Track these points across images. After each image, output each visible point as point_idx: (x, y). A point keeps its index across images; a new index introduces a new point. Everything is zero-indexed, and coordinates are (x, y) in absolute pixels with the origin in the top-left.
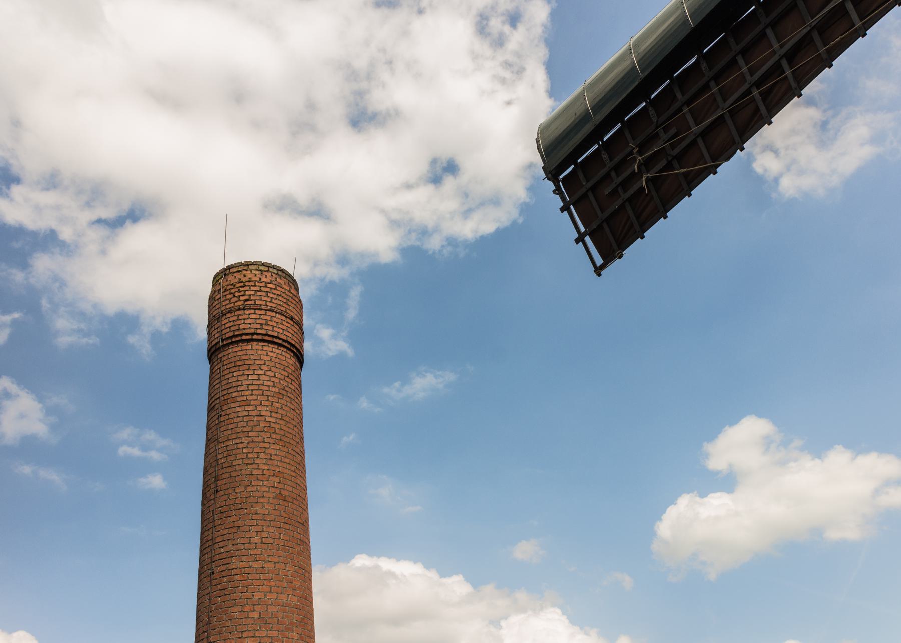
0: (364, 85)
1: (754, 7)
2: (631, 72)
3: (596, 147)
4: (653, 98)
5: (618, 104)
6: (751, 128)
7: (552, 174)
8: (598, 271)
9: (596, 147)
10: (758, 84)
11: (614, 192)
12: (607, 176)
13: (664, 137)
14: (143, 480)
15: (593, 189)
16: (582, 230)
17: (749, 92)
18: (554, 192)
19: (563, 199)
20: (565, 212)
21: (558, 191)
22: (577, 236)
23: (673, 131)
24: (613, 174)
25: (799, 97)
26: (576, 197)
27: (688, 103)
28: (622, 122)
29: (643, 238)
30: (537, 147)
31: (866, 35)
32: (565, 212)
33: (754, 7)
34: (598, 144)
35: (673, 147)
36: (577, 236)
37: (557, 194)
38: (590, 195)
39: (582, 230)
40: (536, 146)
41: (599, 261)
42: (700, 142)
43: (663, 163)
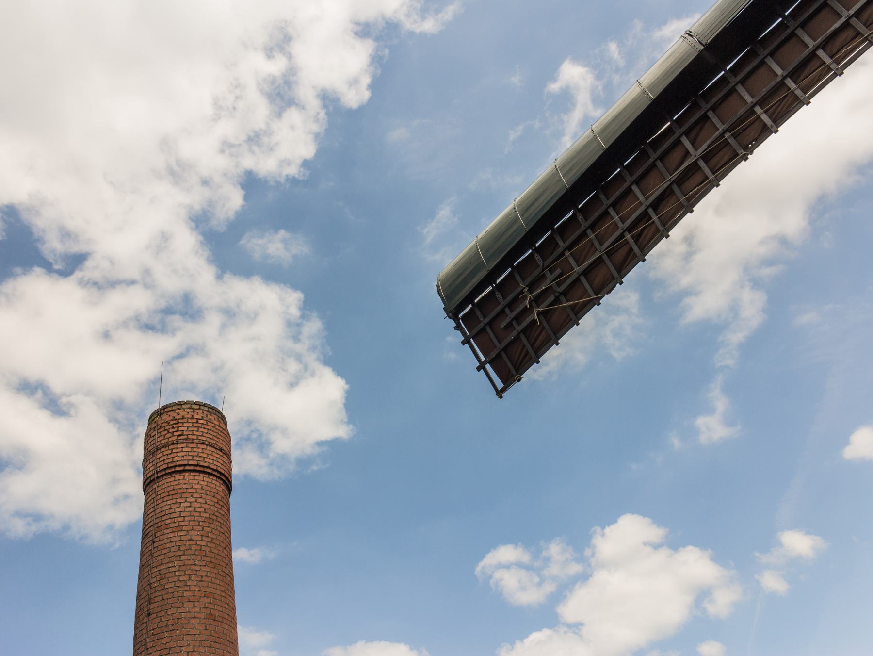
1: (619, 169)
3: (490, 288)
7: (453, 313)
8: (500, 393)
9: (490, 288)
10: (630, 229)
11: (509, 326)
12: (502, 312)
13: (550, 277)
18: (455, 328)
19: (464, 334)
20: (467, 345)
23: (558, 271)
24: (507, 310)
27: (592, 227)
30: (438, 291)
31: (810, 103)
32: (467, 345)
34: (492, 286)
35: (559, 284)
37: (458, 330)
39: (483, 358)
41: (500, 385)
43: (551, 298)
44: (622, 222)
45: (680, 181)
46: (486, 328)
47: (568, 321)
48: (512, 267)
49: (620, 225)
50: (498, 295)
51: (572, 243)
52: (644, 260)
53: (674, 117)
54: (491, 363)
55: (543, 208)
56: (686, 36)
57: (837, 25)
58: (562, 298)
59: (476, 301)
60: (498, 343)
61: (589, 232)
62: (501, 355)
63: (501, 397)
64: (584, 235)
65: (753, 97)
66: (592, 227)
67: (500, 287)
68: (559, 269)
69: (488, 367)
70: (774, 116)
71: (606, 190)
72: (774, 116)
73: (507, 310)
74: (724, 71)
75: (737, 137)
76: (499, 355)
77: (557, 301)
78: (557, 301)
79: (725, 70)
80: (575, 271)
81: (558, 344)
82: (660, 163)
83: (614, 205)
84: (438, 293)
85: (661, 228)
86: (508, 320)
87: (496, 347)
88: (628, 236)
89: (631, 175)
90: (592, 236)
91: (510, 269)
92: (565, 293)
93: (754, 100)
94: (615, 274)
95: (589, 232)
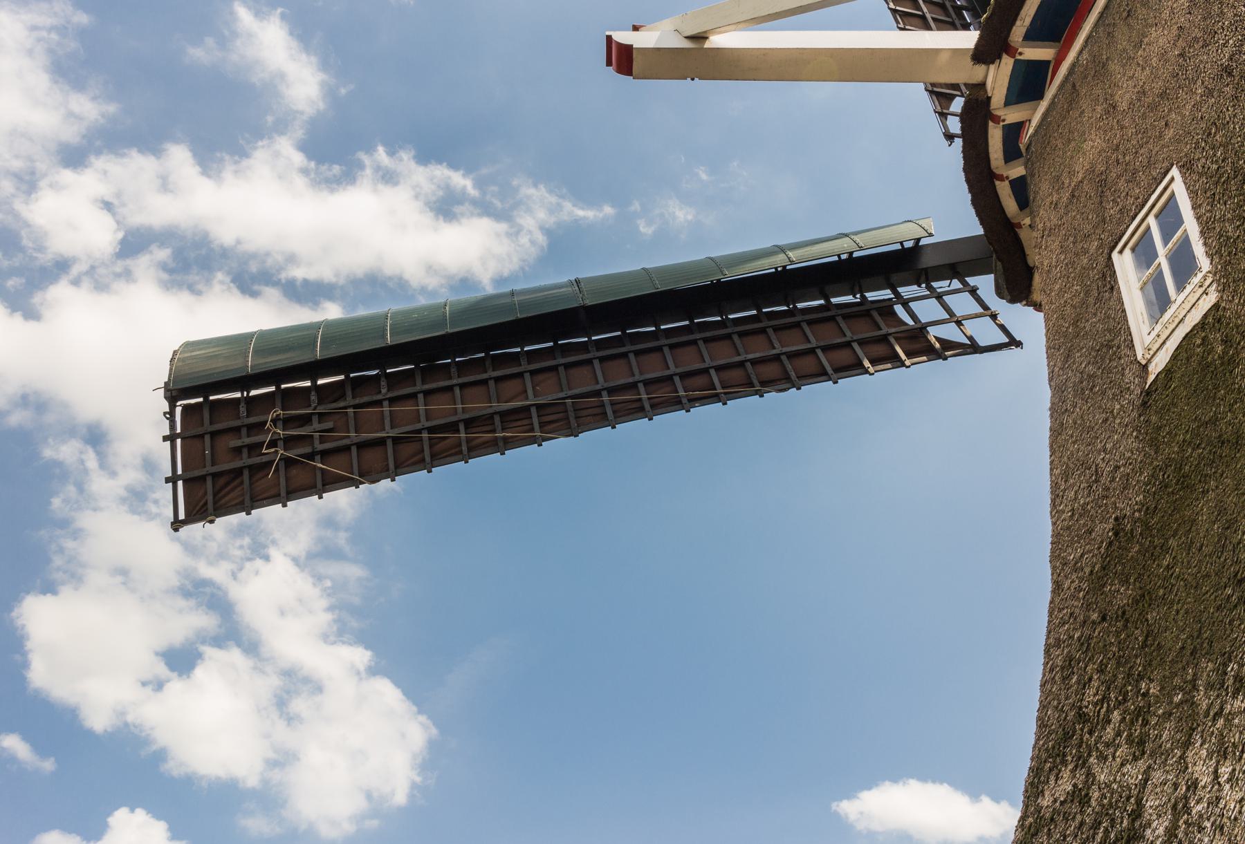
0: (1111, 29)
1: (450, 361)
2: (442, 322)
3: (238, 395)
4: (374, 369)
5: (431, 337)
6: (443, 458)
7: (174, 393)
8: (177, 525)
9: (238, 395)
10: (431, 430)
11: (238, 451)
12: (236, 430)
13: (316, 425)
14: (690, 217)
15: (214, 435)
16: (180, 472)
17: (419, 431)
18: (165, 414)
19: (172, 426)
20: (168, 443)
21: (170, 415)
22: (170, 474)
23: (329, 425)
24: (244, 431)
25: (501, 454)
26: (188, 434)
27: (392, 401)
28: (278, 387)
29: (503, 454)
30: (172, 359)
31: (578, 436)
32: (168, 443)
33: (450, 361)
34: (242, 394)
35: (322, 440)
36: (170, 474)
37: (167, 418)
38: (207, 438)
39: (180, 472)
40: (171, 357)
41: (182, 516)
42: (246, 473)
43: (308, 450)
44: (391, 426)
45: (506, 416)
46: (242, 430)
47: (453, 451)
48: (487, 354)
49: (423, 418)
50: (243, 409)
51: (545, 368)
52: (614, 427)
53: (663, 325)
54: (185, 482)
55: (207, 370)
56: (575, 284)
57: (839, 341)
58: (318, 457)
59: (283, 386)
60: (673, 366)
61: (386, 403)
62: (205, 480)
63: (176, 530)
64: (379, 403)
65: (676, 367)
66: (392, 401)
67: (250, 401)
68: (332, 423)
69: (180, 483)
70: (457, 450)
71: (429, 372)
72: (457, 450)
73: (244, 431)
74: (312, 383)
75: (541, 416)
76: (202, 479)
77: (311, 456)
78: (311, 456)
79: (658, 329)
80: (491, 406)
81: (285, 505)
82: (529, 377)
83: (427, 393)
84: (171, 361)
85: (428, 459)
86: (238, 443)
87: (419, 422)
88: (425, 435)
89: (424, 382)
90: (386, 409)
91: (201, 400)
92: (325, 454)
93: (606, 385)
94: (283, 493)
95: (386, 403)
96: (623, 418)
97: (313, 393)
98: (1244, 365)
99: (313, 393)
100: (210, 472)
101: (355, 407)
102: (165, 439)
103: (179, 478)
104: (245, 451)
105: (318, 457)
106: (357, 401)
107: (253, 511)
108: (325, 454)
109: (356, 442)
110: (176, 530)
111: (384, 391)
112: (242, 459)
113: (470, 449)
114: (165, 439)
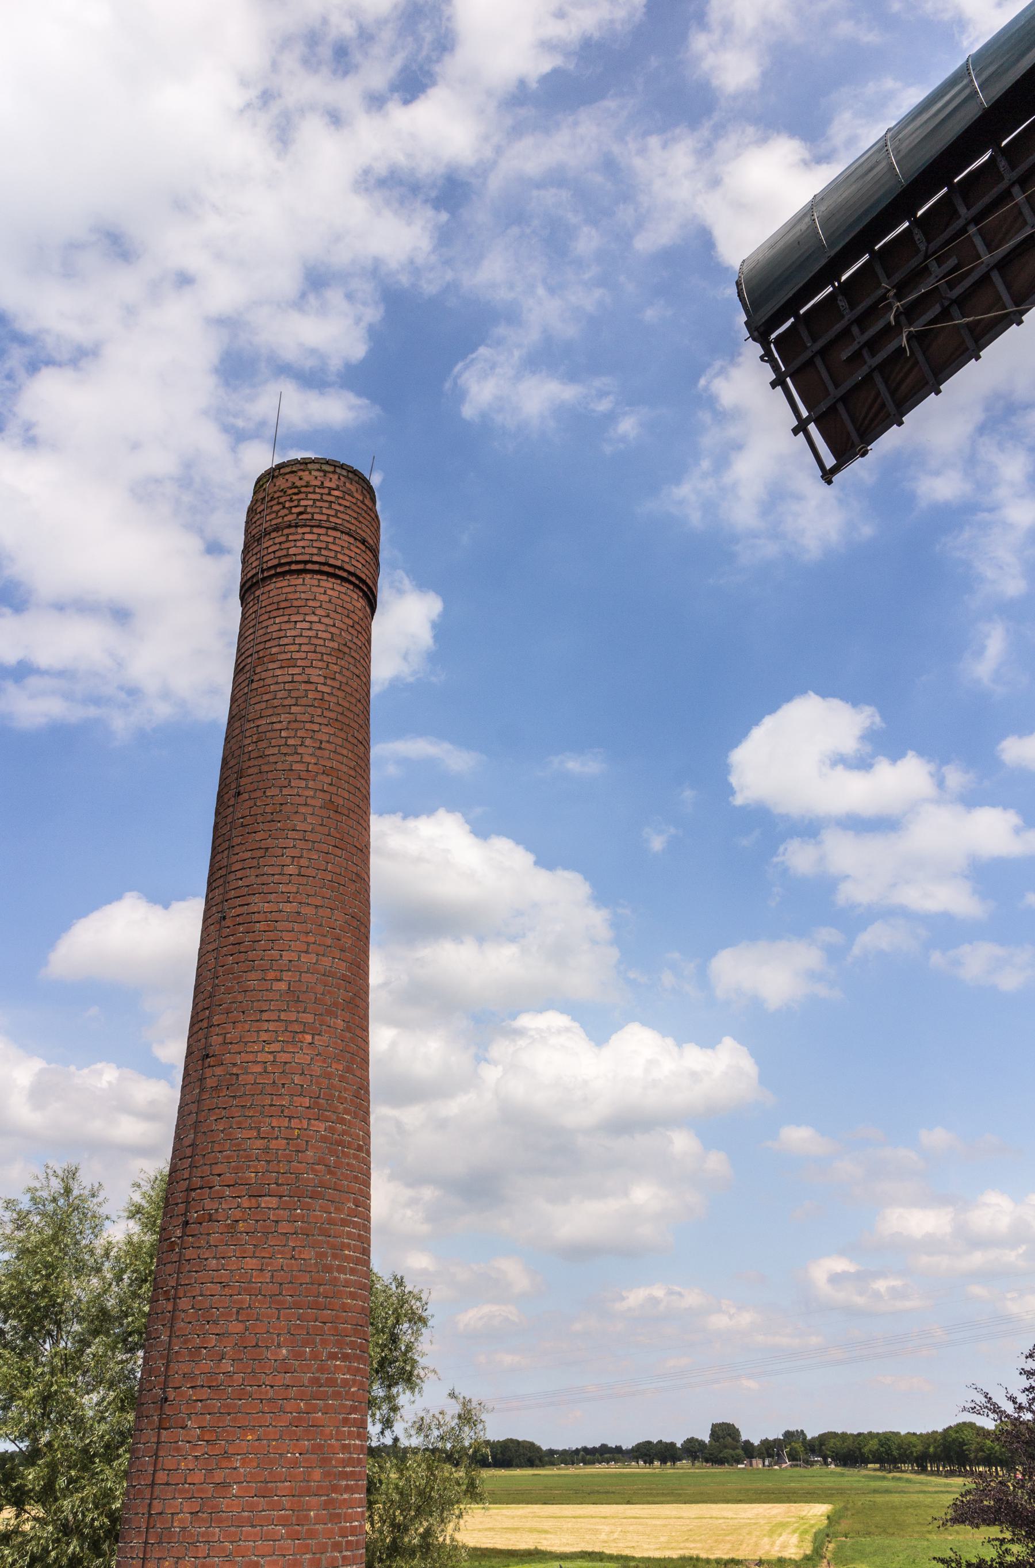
8: (828, 475)
11: (856, 357)
19: (775, 368)
20: (779, 388)
23: (952, 262)
24: (855, 330)
30: (738, 293)
32: (779, 388)
34: (833, 286)
35: (951, 285)
37: (766, 361)
38: (818, 361)
39: (805, 413)
41: (830, 461)
43: (936, 309)
50: (842, 303)
58: (955, 311)
59: (802, 312)
61: (1016, 190)
63: (829, 482)
69: (812, 428)
77: (945, 315)
81: (938, 392)
90: (1020, 198)
91: (867, 256)
92: (961, 302)
95: (1016, 190)
96: (987, 337)
97: (840, 298)
98: (316, 1564)
99: (840, 298)
100: (874, 365)
101: (976, 220)
102: (774, 385)
103: (808, 421)
104: (865, 353)
105: (955, 311)
106: (974, 211)
107: (981, 353)
108: (961, 302)
109: (839, 395)
110: (829, 482)
111: (923, 247)
112: (865, 363)
113: (976, 340)
114: (774, 385)
